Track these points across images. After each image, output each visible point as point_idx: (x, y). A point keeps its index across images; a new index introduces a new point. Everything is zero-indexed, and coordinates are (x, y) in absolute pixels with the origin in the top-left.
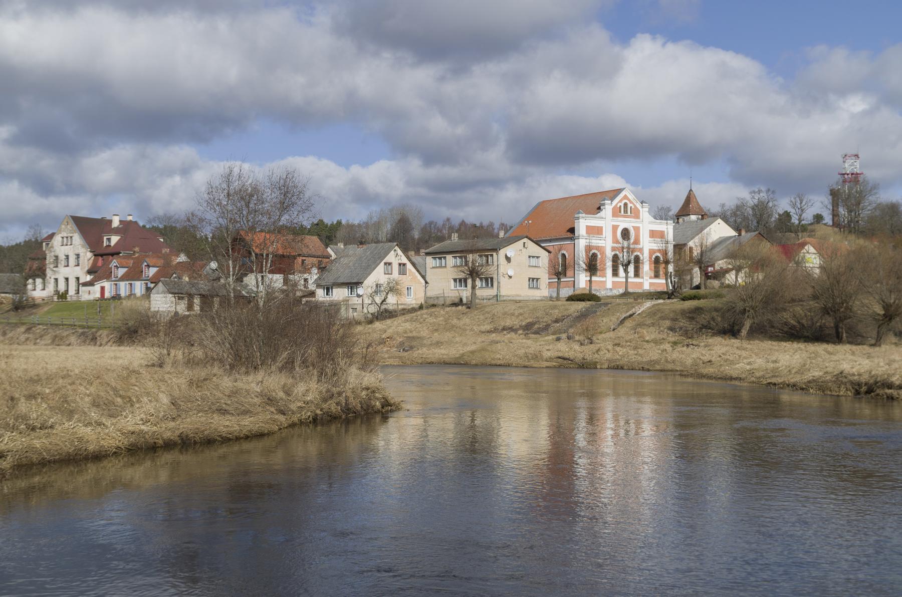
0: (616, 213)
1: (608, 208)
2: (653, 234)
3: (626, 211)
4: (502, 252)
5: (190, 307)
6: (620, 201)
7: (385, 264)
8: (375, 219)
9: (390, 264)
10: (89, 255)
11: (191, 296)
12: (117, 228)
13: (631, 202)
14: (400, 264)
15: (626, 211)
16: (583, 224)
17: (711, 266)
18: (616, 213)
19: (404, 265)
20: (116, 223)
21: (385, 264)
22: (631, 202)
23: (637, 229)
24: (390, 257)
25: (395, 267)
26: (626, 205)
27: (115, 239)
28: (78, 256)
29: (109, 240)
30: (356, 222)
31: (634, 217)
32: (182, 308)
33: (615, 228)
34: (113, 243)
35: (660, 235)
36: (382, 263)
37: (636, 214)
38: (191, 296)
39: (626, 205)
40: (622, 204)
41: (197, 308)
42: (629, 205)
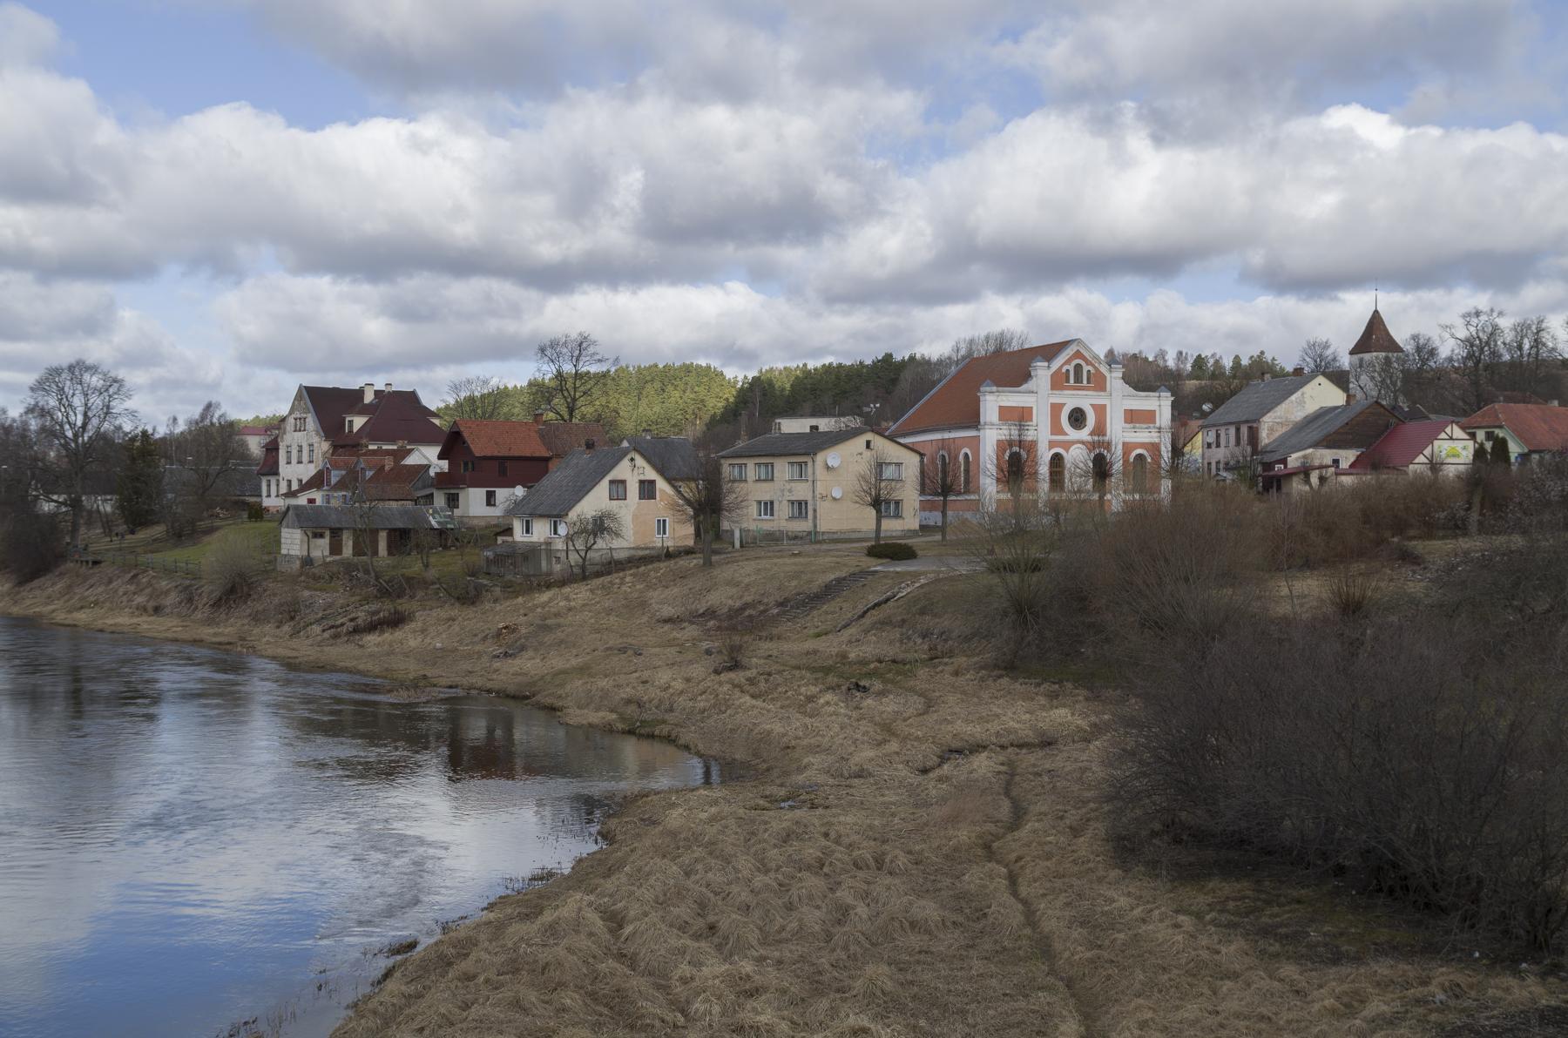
0: (1059, 382)
1: (1042, 373)
2: (1132, 417)
3: (1078, 379)
4: (820, 457)
5: (336, 548)
6: (1068, 362)
7: (611, 482)
8: (963, 352)
9: (623, 482)
10: (325, 446)
11: (336, 533)
12: (370, 405)
13: (1088, 363)
14: (642, 482)
15: (1078, 379)
16: (992, 402)
17: (1279, 462)
18: (1059, 382)
19: (653, 482)
20: (369, 398)
21: (611, 482)
22: (1088, 363)
23: (1100, 410)
24: (623, 470)
25: (633, 489)
26: (1078, 368)
27: (359, 422)
28: (311, 445)
29: (351, 422)
30: (935, 358)
31: (1096, 389)
32: (321, 549)
33: (1056, 409)
34: (356, 428)
35: (1146, 418)
36: (605, 483)
37: (1099, 383)
38: (336, 533)
39: (1078, 368)
40: (1071, 368)
41: (348, 550)
42: (1086, 368)
